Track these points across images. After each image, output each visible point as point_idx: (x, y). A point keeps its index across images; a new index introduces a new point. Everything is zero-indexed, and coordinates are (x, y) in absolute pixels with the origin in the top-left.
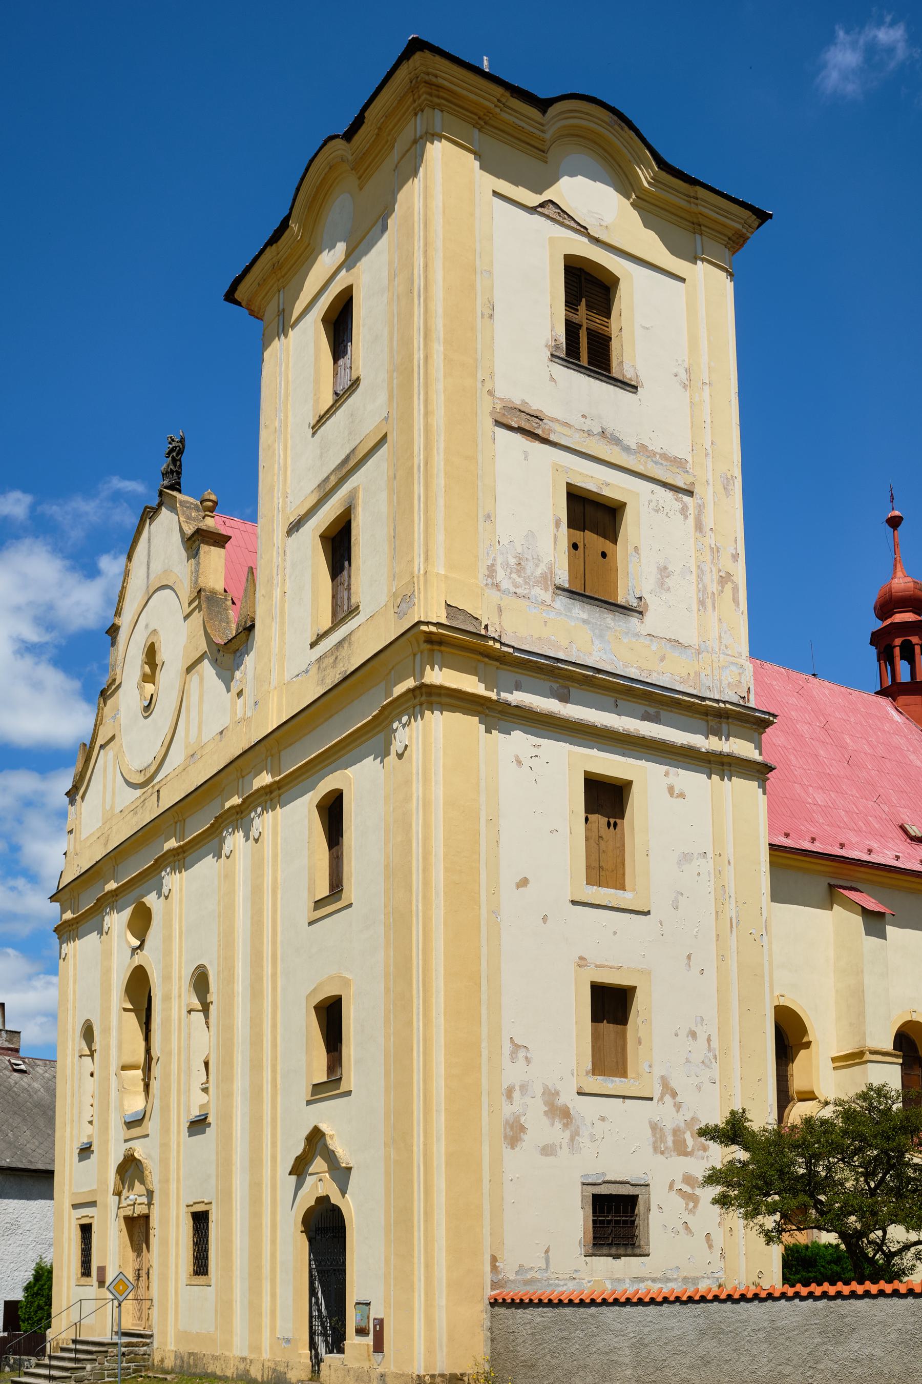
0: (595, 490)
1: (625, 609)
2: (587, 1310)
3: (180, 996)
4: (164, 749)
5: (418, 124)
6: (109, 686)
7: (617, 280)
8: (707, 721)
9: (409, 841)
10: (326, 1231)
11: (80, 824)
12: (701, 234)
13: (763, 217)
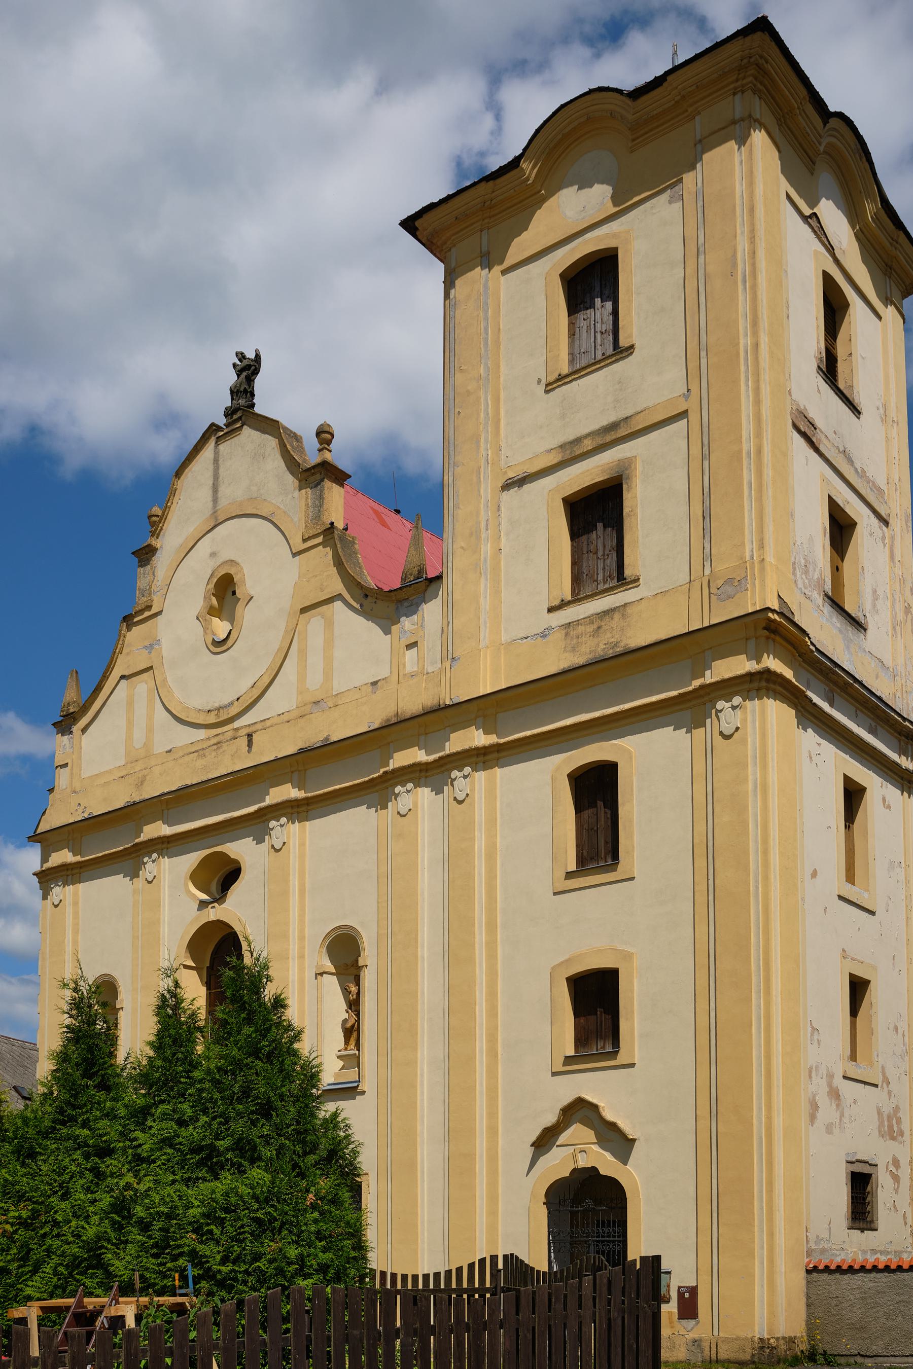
0: (842, 506)
2: (869, 1275)
3: (302, 957)
4: (256, 693)
5: (738, 106)
6: (141, 612)
8: (899, 741)
9: (744, 824)
11: (80, 758)
12: (890, 277)
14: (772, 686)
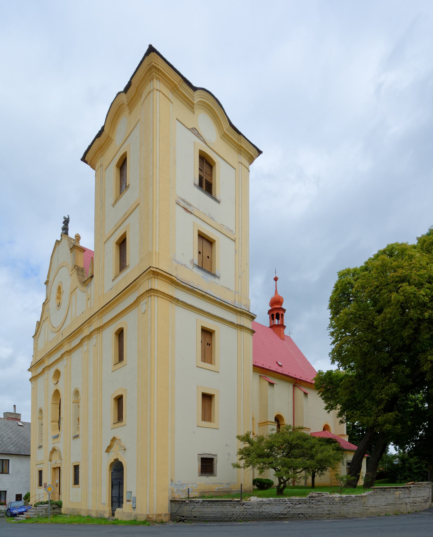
1: (214, 275)
7: (215, 163)
10: (117, 469)
13: (260, 152)
14: (155, 294)
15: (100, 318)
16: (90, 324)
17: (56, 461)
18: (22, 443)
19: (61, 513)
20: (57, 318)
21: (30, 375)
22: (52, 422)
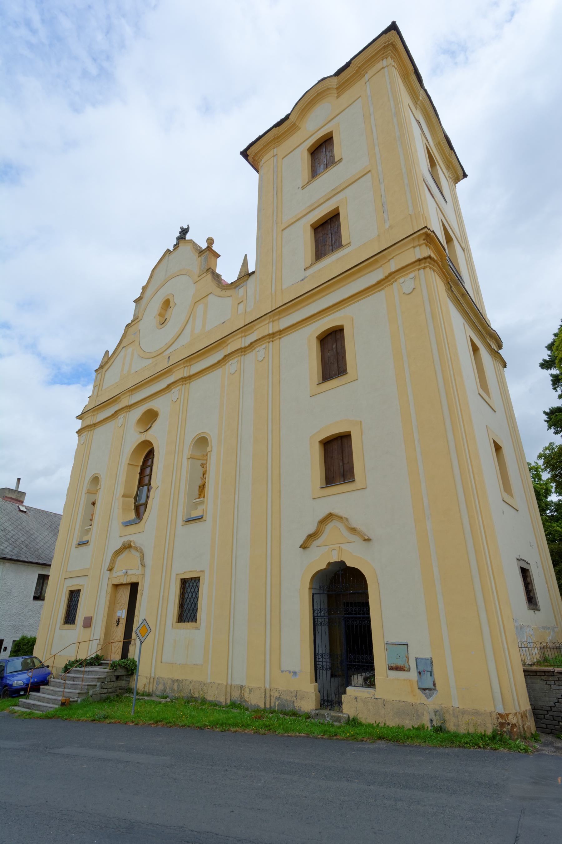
13: (465, 176)
14: (431, 266)
15: (273, 321)
16: (247, 334)
17: (127, 569)
18: (23, 539)
19: (129, 690)
20: (154, 339)
21: (79, 424)
22: (123, 496)
